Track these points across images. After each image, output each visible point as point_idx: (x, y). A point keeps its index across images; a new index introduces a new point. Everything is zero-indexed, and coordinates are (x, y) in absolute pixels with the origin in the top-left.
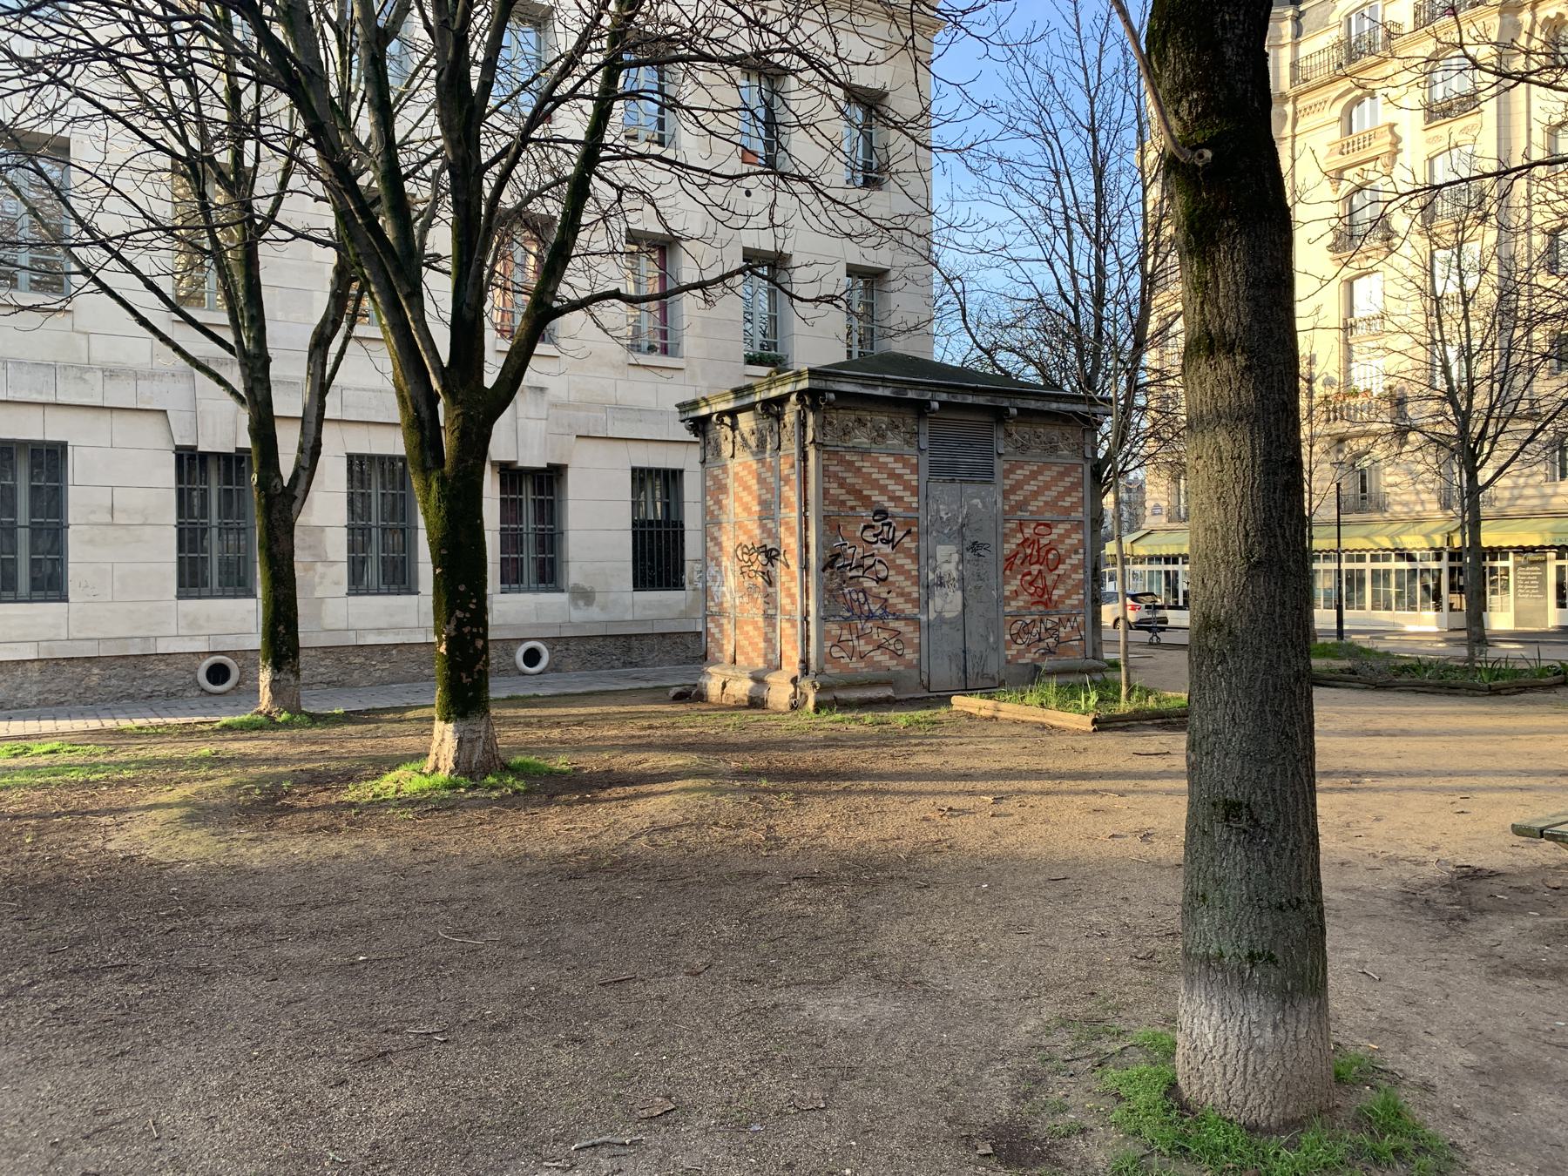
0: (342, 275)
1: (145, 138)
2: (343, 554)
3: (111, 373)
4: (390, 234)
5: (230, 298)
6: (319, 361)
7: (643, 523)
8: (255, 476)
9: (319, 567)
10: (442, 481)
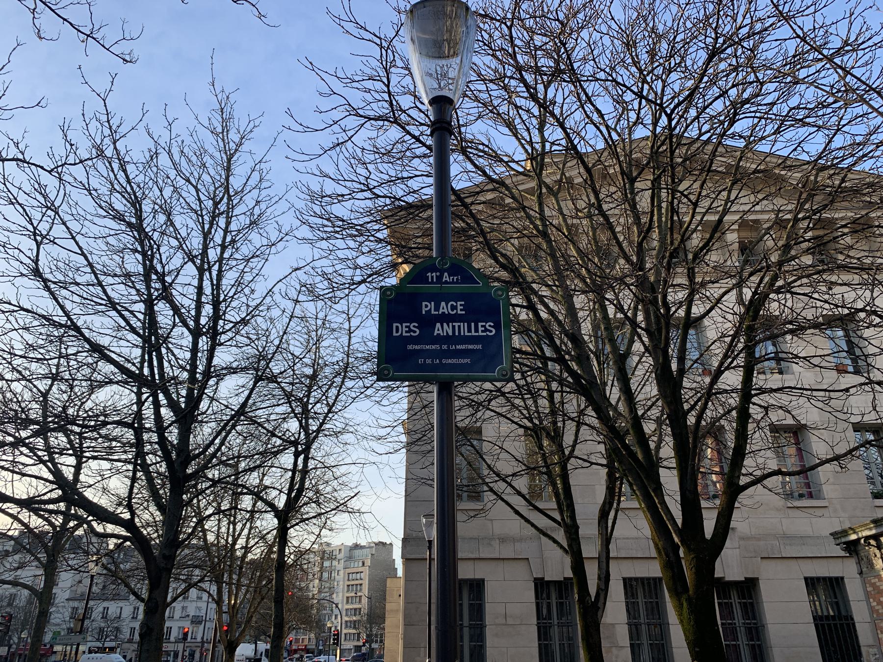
0: (611, 476)
1: (513, 422)
2: (627, 643)
3: (503, 540)
4: (640, 456)
5: (557, 495)
6: (604, 525)
7: (821, 618)
8: (576, 596)
9: (614, 650)
10: (689, 600)
